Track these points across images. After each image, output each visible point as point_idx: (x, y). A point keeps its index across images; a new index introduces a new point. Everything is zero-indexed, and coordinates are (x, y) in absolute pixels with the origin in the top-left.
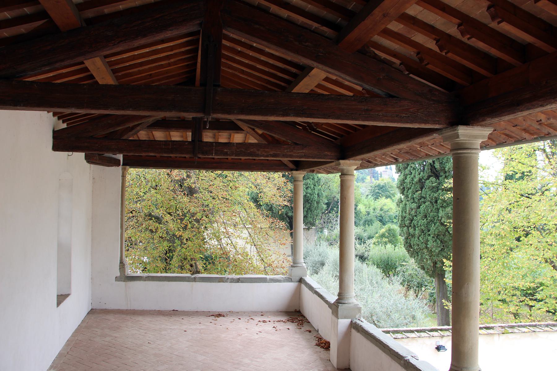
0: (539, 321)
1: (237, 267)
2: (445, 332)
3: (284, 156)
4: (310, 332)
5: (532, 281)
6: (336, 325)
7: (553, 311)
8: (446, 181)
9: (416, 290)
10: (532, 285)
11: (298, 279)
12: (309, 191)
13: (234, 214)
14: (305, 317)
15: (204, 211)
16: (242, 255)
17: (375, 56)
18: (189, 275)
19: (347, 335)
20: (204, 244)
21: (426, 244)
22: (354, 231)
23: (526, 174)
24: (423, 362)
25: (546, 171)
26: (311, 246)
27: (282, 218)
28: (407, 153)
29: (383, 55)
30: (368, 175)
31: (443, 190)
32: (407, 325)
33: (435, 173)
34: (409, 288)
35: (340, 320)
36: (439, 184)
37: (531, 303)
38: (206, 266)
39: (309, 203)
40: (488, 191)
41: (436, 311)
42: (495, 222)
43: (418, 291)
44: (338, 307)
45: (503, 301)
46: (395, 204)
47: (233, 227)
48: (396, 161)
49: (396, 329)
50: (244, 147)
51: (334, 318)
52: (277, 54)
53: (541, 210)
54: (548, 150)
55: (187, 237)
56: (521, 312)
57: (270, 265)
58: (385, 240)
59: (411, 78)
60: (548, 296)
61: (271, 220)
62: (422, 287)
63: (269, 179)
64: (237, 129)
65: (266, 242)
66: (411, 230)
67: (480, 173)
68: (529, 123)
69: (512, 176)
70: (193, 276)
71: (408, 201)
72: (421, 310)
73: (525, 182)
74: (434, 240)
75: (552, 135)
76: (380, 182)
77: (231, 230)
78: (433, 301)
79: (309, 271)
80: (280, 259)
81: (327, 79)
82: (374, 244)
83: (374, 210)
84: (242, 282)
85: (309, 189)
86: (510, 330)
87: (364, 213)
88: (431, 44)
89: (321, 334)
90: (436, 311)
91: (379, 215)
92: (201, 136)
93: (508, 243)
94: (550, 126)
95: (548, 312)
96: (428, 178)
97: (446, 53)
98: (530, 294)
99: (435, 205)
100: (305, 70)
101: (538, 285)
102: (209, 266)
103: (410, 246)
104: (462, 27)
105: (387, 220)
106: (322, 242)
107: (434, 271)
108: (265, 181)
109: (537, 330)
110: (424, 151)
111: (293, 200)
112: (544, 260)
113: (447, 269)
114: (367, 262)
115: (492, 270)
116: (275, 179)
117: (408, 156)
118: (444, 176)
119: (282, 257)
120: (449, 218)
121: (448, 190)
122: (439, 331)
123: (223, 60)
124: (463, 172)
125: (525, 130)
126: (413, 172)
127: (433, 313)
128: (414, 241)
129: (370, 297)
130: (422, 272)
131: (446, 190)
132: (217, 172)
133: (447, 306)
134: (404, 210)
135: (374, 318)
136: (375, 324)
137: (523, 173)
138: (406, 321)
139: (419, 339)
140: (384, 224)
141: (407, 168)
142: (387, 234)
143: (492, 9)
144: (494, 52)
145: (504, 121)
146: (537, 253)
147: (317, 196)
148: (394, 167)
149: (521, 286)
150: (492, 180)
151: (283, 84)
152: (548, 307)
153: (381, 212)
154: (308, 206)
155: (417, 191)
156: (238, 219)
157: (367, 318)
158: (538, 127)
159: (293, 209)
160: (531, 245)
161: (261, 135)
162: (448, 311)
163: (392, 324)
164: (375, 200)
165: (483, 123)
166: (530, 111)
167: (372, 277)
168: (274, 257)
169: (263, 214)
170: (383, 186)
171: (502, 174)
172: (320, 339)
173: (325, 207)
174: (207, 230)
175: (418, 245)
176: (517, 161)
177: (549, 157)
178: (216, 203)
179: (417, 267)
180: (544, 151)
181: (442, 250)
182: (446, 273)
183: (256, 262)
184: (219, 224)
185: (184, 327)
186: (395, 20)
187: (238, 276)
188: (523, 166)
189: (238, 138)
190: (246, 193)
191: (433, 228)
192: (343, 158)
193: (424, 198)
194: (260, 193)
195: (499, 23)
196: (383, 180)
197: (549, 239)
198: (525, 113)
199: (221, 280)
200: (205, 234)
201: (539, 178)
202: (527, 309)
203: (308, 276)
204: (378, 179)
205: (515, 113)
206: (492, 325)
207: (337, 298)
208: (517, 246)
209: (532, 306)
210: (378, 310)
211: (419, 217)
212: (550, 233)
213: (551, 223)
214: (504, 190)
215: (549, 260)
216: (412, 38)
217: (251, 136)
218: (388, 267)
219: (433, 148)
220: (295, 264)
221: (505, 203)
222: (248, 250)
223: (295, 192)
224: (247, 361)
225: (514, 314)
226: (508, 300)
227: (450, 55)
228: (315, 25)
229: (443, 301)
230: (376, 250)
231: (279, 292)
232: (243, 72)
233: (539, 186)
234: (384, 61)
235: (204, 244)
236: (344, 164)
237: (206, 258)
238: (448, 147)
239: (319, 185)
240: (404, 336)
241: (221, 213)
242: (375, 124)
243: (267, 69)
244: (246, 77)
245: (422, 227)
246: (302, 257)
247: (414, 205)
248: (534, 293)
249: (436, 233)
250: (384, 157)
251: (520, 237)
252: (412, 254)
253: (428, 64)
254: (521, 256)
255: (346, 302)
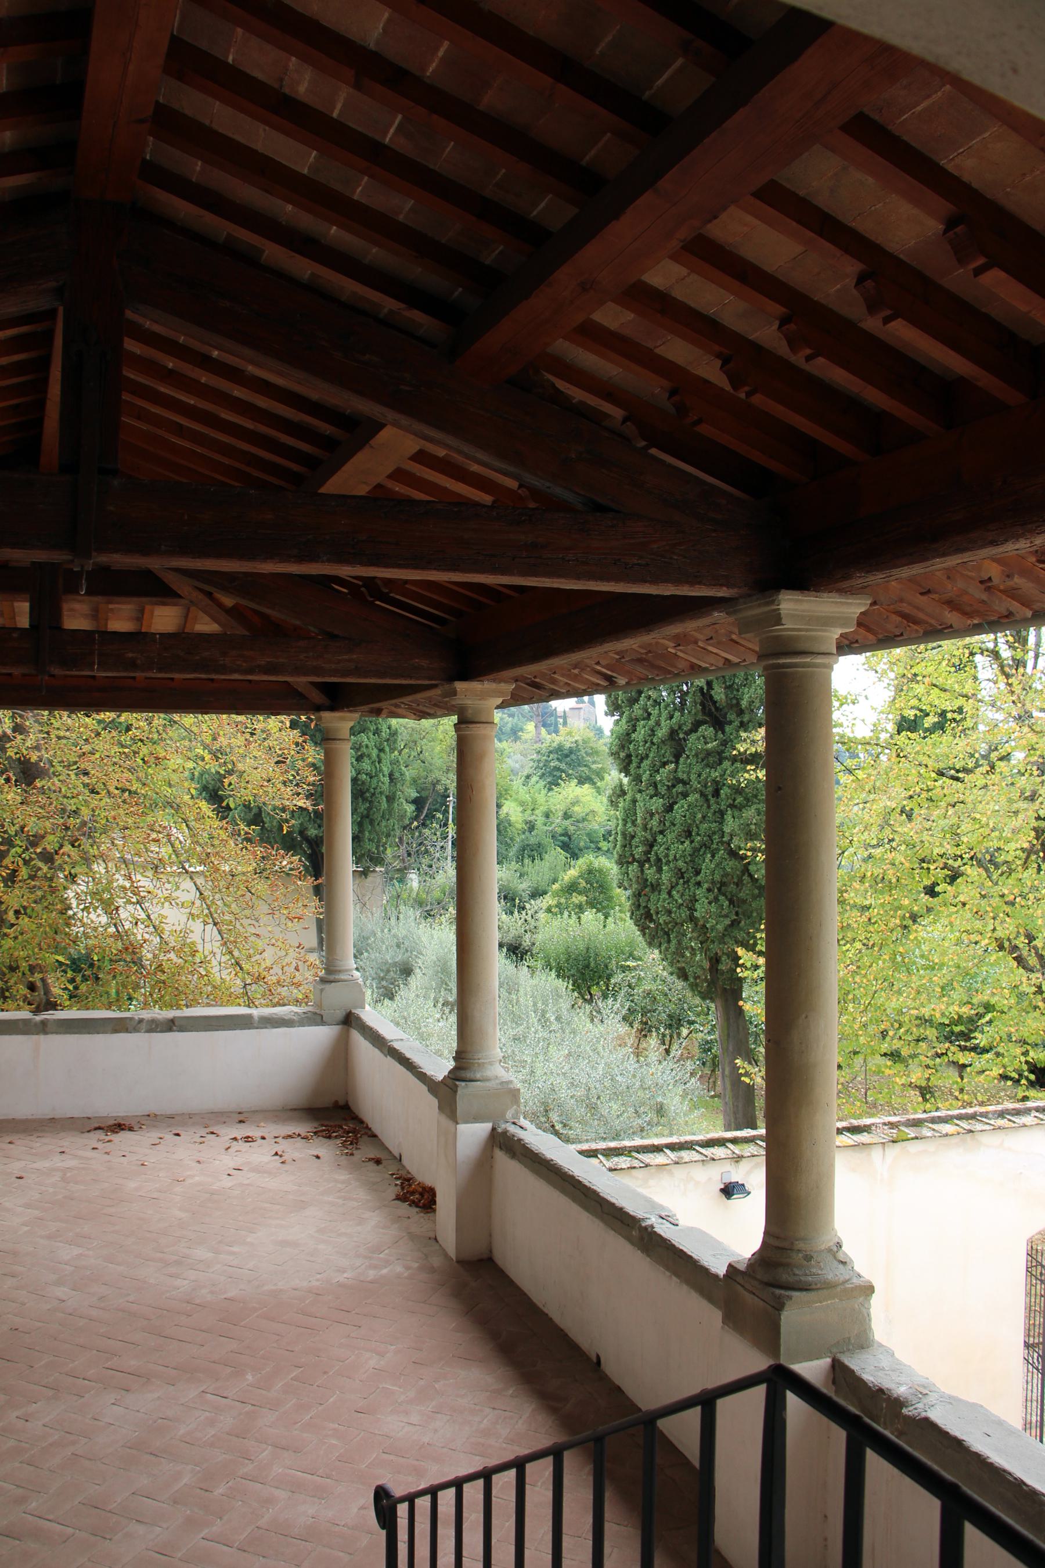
0: (982, 1104)
1: (167, 986)
2: (746, 1146)
3: (298, 671)
4: (378, 1162)
5: (965, 1000)
6: (450, 1141)
7: (1015, 1075)
8: (744, 735)
9: (664, 1035)
10: (966, 1011)
11: (340, 1014)
12: (366, 765)
13: (154, 835)
14: (362, 1122)
15: (67, 828)
16: (179, 952)
17: (557, 398)
18: (25, 1014)
19: (483, 1167)
20: (68, 925)
21: (692, 909)
22: (496, 875)
23: (949, 716)
24: (691, 1229)
25: (1000, 709)
26: (373, 921)
27: (289, 844)
28: (640, 661)
29: (577, 394)
30: (530, 719)
31: (734, 760)
32: (642, 1130)
33: (715, 715)
34: (645, 1031)
35: (462, 1127)
36: (724, 743)
37: (963, 1058)
38: (76, 988)
39: (365, 800)
40: (855, 761)
41: (719, 1088)
42: (874, 847)
43: (671, 1037)
44: (454, 1090)
45: (894, 1056)
46: (605, 800)
47: (150, 873)
48: (608, 685)
49: (613, 1144)
50: (181, 642)
51: (446, 1122)
52: (280, 381)
53: (995, 815)
54: (1006, 653)
55: (17, 907)
56: (940, 1083)
57: (259, 979)
58: (577, 899)
59: (654, 458)
60: (1005, 1037)
61: (260, 851)
62: (679, 1025)
63: (252, 734)
64: (163, 592)
65: (247, 912)
66: (650, 872)
67: (836, 716)
68: (960, 584)
69: (915, 721)
70: (38, 1018)
71: (640, 791)
72: (680, 1090)
73: (946, 738)
74: (711, 897)
75: (1018, 617)
76: (563, 738)
77: (144, 881)
78: (711, 1064)
79: (369, 992)
80: (287, 960)
81: (420, 457)
82: (549, 910)
83: (547, 816)
84: (182, 1029)
85: (366, 759)
86: (911, 1132)
87: (519, 826)
88: (707, 368)
89: (408, 1167)
90: (719, 1088)
91: (559, 830)
92: (56, 615)
93: (906, 902)
94: (1012, 593)
95: (1004, 1077)
96: (695, 729)
97: (748, 394)
98: (962, 1033)
99: (712, 801)
100: (359, 431)
101: (981, 1010)
102: (83, 988)
103: (648, 916)
104: (792, 327)
105: (582, 844)
106: (402, 908)
107: (712, 983)
108: (240, 740)
109: (979, 1127)
110: (686, 655)
111: (323, 793)
112: (994, 944)
113: (746, 973)
114: (529, 961)
115: (865, 976)
116: (269, 735)
117: (640, 670)
118: (737, 723)
119: (292, 954)
120: (751, 836)
121: (752, 759)
122: (729, 1145)
123: (126, 397)
124: (793, 713)
125: (952, 604)
126: (655, 712)
127: (712, 1097)
128: (658, 902)
129: (541, 1058)
130: (680, 984)
131: (742, 761)
132: (102, 716)
133: (747, 1074)
134: (629, 816)
135: (554, 1117)
136: (557, 1133)
137: (943, 714)
138: (640, 1121)
139: (678, 1171)
140: (575, 856)
141: (637, 700)
142: (583, 883)
143: (869, 284)
144: (874, 396)
145: (898, 580)
146: (978, 925)
147: (387, 780)
148: (600, 699)
149: (938, 1015)
150: (863, 732)
151: (294, 467)
152: (1004, 1067)
153: (567, 823)
154: (363, 807)
155: (664, 764)
156: (165, 851)
157: (534, 1118)
158: (984, 596)
159: (323, 818)
160: (964, 904)
161: (233, 612)
162: (750, 1089)
163: (601, 1131)
164: (550, 789)
165: (845, 584)
166: (966, 557)
167: (545, 1003)
168: (269, 956)
169: (236, 834)
170: (571, 751)
171: (890, 716)
172: (407, 1180)
173: (410, 809)
174: (74, 882)
175: (669, 912)
176: (926, 680)
177: (1007, 669)
178: (103, 803)
179: (665, 973)
180: (995, 654)
181: (734, 924)
182: (745, 986)
183: (220, 971)
184: (110, 865)
185: (16, 1167)
186: (612, 301)
187: (171, 1014)
188: (943, 694)
189: (164, 619)
190: (187, 774)
191: (707, 864)
192: (465, 677)
193: (685, 783)
194: (230, 772)
195: (887, 320)
196: (570, 734)
197: (1008, 887)
198: (953, 561)
199: (120, 1026)
200: (70, 894)
201: (982, 728)
202: (953, 1074)
203: (367, 1007)
204: (556, 732)
205: (927, 559)
206: (867, 1121)
207: (451, 1064)
208: (929, 910)
209: (964, 1066)
210: (563, 1094)
211: (670, 836)
212: (1011, 871)
213: (1013, 846)
214: (894, 759)
215: (1006, 944)
216: (657, 351)
217: (201, 614)
218: (587, 974)
219: (710, 648)
220: (331, 974)
221: (895, 797)
222: (195, 937)
223: (328, 770)
224: (201, 1253)
225: (920, 1088)
226: (905, 1052)
227: (757, 399)
228: (389, 304)
229: (738, 1062)
230: (554, 929)
231: (294, 1052)
232: (180, 430)
233: (983, 748)
234: (582, 412)
235: (68, 925)
236: (469, 692)
237: (75, 965)
238: (750, 645)
239: (392, 750)
240: (636, 1163)
241: (116, 834)
242: (555, 586)
243: (249, 424)
244: (188, 445)
245: (680, 864)
246: (351, 951)
247: (657, 804)
248: (971, 1031)
249: (717, 878)
250: (576, 671)
251: (935, 884)
252: (653, 938)
253: (700, 421)
254: (936, 934)
255: (478, 1076)
